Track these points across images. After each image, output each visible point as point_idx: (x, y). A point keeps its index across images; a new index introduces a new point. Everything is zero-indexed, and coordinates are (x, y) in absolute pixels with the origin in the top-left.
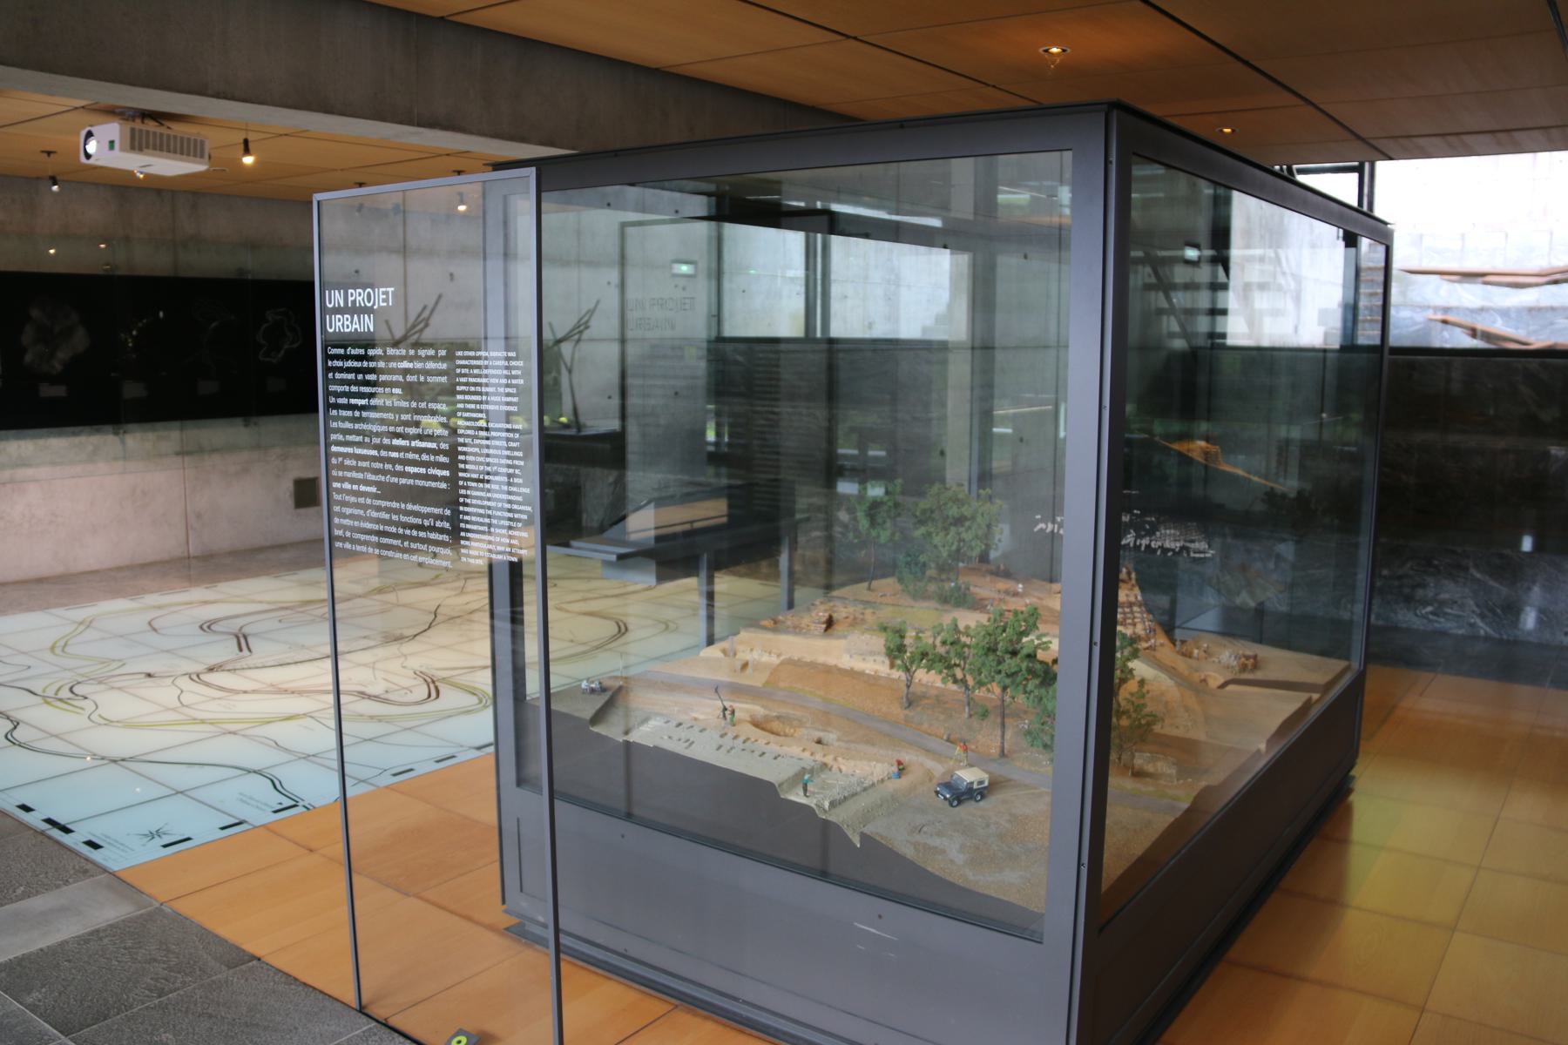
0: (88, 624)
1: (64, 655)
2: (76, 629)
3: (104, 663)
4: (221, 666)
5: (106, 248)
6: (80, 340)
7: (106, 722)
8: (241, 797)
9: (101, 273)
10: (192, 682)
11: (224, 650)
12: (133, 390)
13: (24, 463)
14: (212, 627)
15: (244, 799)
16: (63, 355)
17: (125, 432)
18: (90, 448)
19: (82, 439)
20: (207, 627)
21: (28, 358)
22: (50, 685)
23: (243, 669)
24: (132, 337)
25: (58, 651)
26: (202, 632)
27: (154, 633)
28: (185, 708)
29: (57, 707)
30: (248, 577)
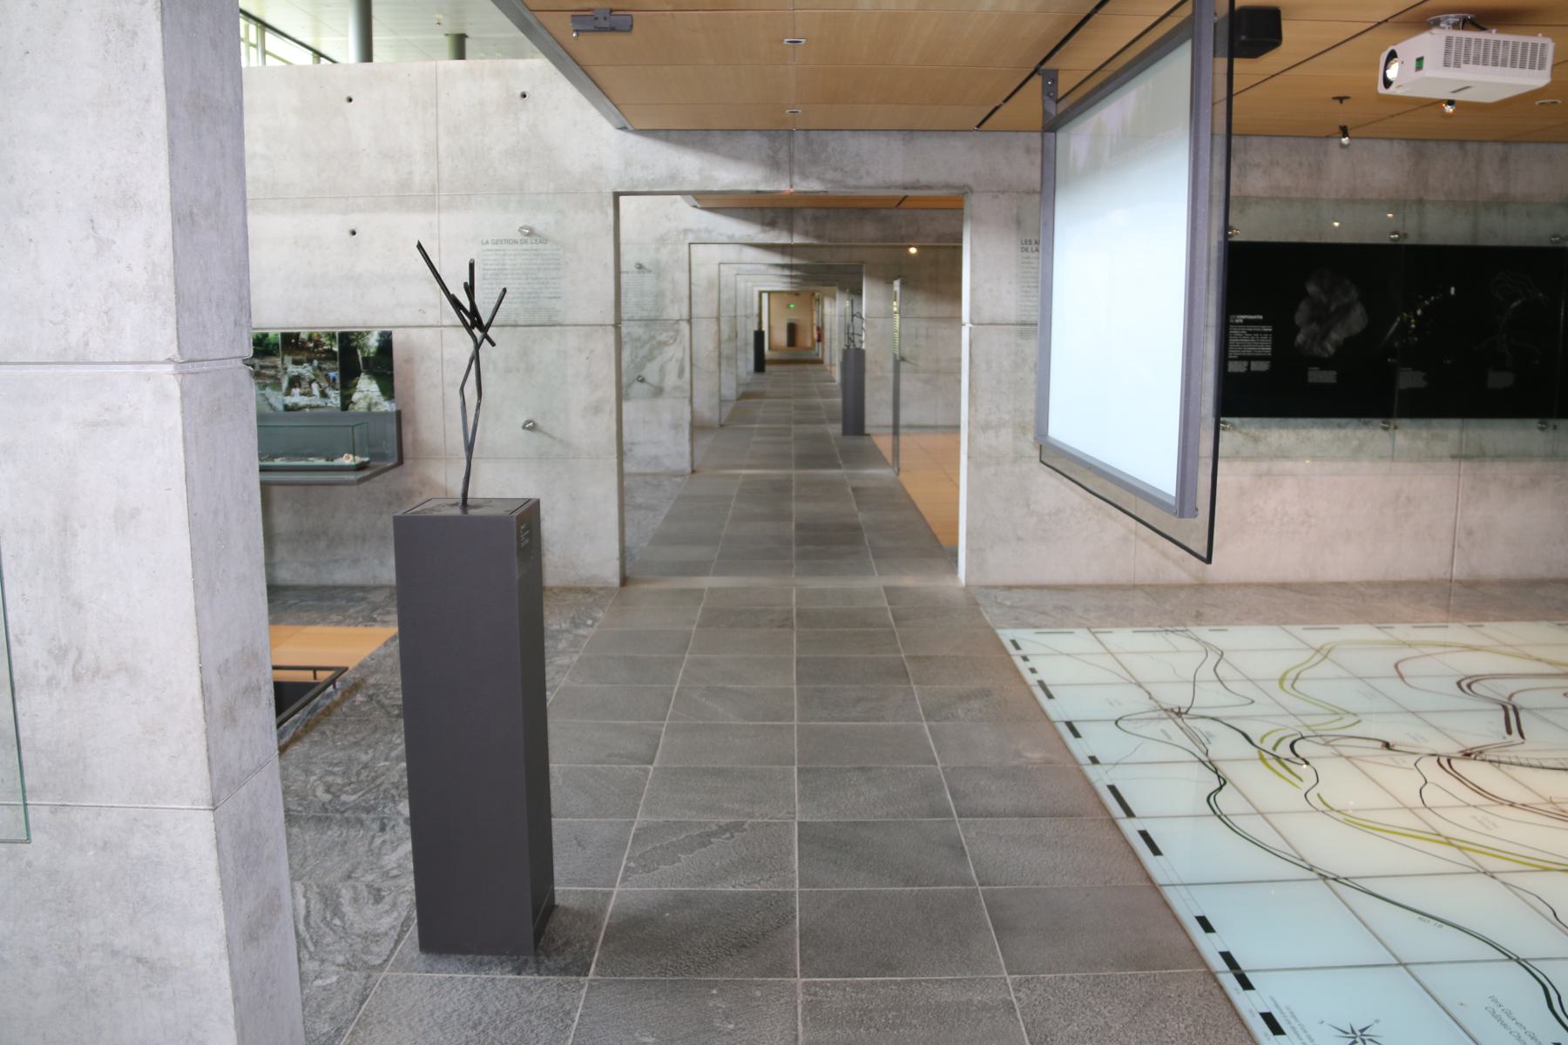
0: (1324, 653)
1: (1292, 691)
2: (1310, 659)
3: (1337, 714)
4: (1481, 752)
5: (1393, 217)
6: (1357, 320)
7: (1324, 808)
8: (1492, 1005)
9: (1387, 242)
10: (1438, 767)
11: (1484, 728)
12: (1410, 379)
13: (1282, 454)
14: (1474, 687)
15: (1498, 1011)
16: (1336, 336)
17: (1396, 428)
18: (1355, 443)
19: (1349, 432)
20: (1466, 685)
21: (1300, 338)
22: (1272, 732)
23: (1512, 764)
24: (1416, 316)
25: (1287, 684)
26: (1459, 691)
27: (1399, 680)
28: (1426, 810)
29: (1272, 769)
30: (1523, 619)
